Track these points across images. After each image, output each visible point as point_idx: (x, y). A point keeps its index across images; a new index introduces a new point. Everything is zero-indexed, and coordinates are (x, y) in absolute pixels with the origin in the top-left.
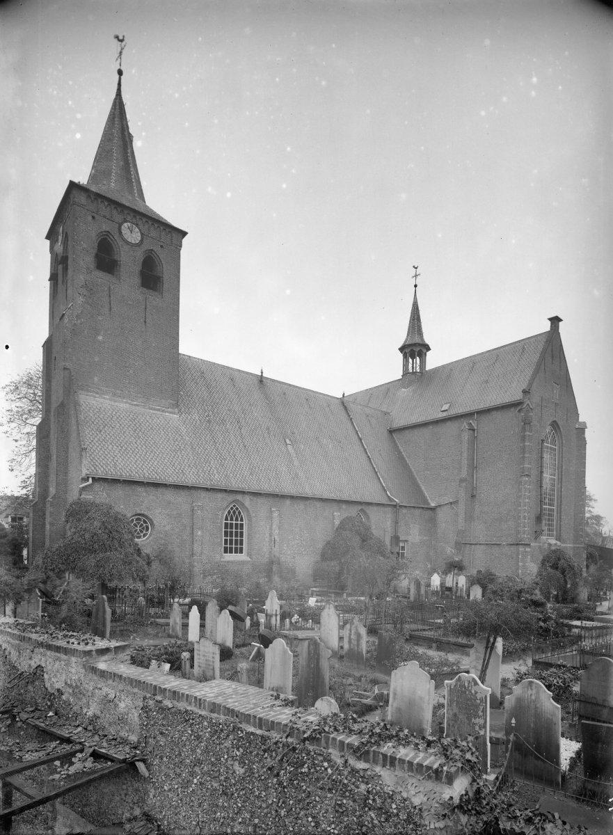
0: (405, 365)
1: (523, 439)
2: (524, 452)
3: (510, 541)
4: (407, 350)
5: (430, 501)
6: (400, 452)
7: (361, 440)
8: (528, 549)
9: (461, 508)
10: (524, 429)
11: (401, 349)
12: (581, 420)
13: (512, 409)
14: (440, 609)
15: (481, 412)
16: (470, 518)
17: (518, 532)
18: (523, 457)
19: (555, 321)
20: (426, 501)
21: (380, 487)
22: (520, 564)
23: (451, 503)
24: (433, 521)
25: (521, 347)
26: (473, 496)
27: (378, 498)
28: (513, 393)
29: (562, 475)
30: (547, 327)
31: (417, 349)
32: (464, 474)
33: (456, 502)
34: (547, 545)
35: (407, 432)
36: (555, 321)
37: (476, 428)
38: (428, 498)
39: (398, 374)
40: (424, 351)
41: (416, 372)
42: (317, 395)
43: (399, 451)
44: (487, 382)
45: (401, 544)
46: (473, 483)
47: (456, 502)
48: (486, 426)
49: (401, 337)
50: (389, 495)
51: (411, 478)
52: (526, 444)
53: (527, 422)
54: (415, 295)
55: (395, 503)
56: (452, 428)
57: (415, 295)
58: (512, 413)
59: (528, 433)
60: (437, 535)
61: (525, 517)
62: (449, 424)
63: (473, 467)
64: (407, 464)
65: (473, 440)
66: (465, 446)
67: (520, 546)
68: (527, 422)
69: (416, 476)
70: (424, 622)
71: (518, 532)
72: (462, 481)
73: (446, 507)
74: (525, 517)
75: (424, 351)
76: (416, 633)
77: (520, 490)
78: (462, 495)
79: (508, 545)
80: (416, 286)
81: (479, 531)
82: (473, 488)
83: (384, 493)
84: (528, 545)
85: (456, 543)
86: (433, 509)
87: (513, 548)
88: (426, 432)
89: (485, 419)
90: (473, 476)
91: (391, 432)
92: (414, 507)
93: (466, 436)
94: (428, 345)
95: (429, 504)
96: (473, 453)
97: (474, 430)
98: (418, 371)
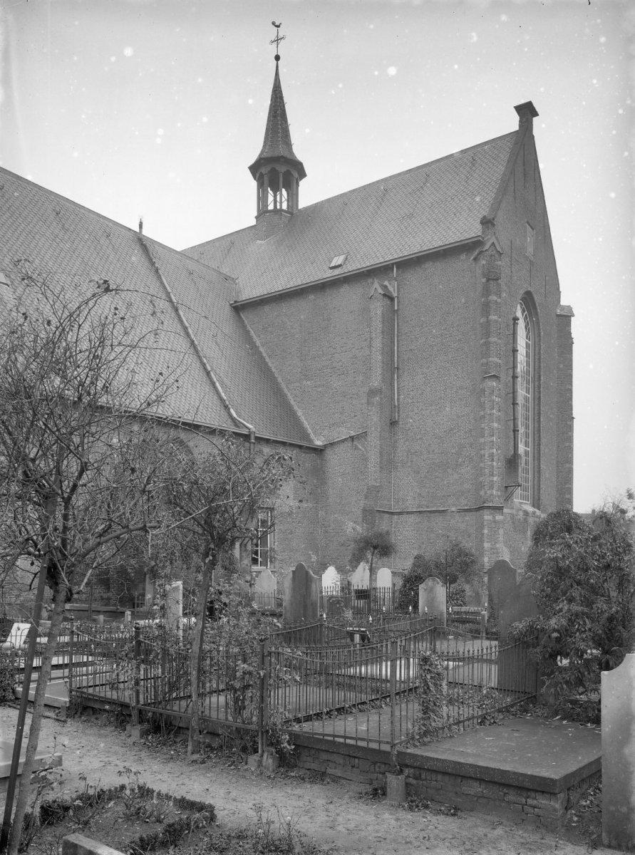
0: (262, 199)
1: (486, 308)
2: (488, 335)
3: (464, 503)
4: (264, 170)
5: (312, 436)
6: (254, 346)
7: (176, 310)
8: (499, 517)
9: (374, 440)
10: (486, 292)
11: (254, 169)
12: (563, 302)
13: (463, 257)
14: (357, 637)
15: (406, 264)
16: (388, 464)
17: (481, 486)
18: (487, 344)
19: (527, 112)
20: (306, 436)
21: (218, 403)
22: (486, 545)
23: (352, 438)
24: (319, 473)
25: (473, 156)
26: (393, 423)
27: (210, 416)
28: (466, 228)
29: (540, 392)
30: (512, 123)
31: (282, 169)
32: (376, 382)
33: (363, 435)
34: (521, 513)
35: (267, 308)
36: (527, 112)
37: (395, 295)
38: (310, 431)
39: (248, 217)
40: (296, 175)
41: (281, 210)
42: (82, 211)
43: (254, 343)
44: (411, 216)
45: (261, 516)
46: (393, 399)
47: (363, 435)
48: (415, 287)
49: (254, 147)
50: (235, 415)
51: (278, 393)
52: (493, 317)
53: (492, 277)
54: (277, 74)
55: (245, 432)
56: (349, 297)
57: (277, 74)
58: (464, 261)
59: (495, 298)
60: (328, 499)
61: (492, 455)
62: (345, 289)
63: (392, 369)
64: (269, 369)
65: (392, 315)
66: (378, 324)
67: (486, 512)
68: (492, 277)
69: (286, 391)
70: (326, 677)
71: (481, 486)
72: (372, 393)
73: (342, 446)
74: (492, 455)
75: (296, 175)
76: (316, 727)
77: (482, 406)
78: (375, 420)
79: (460, 511)
80: (277, 58)
81: (407, 491)
82: (394, 408)
83: (223, 413)
84: (500, 509)
85: (364, 510)
86: (319, 451)
87: (469, 517)
88: (300, 311)
89: (413, 278)
90: (392, 385)
91: (239, 308)
92: (284, 444)
93: (378, 308)
94: (301, 164)
95: (311, 441)
96: (393, 342)
97: (392, 299)
98: (285, 206)
